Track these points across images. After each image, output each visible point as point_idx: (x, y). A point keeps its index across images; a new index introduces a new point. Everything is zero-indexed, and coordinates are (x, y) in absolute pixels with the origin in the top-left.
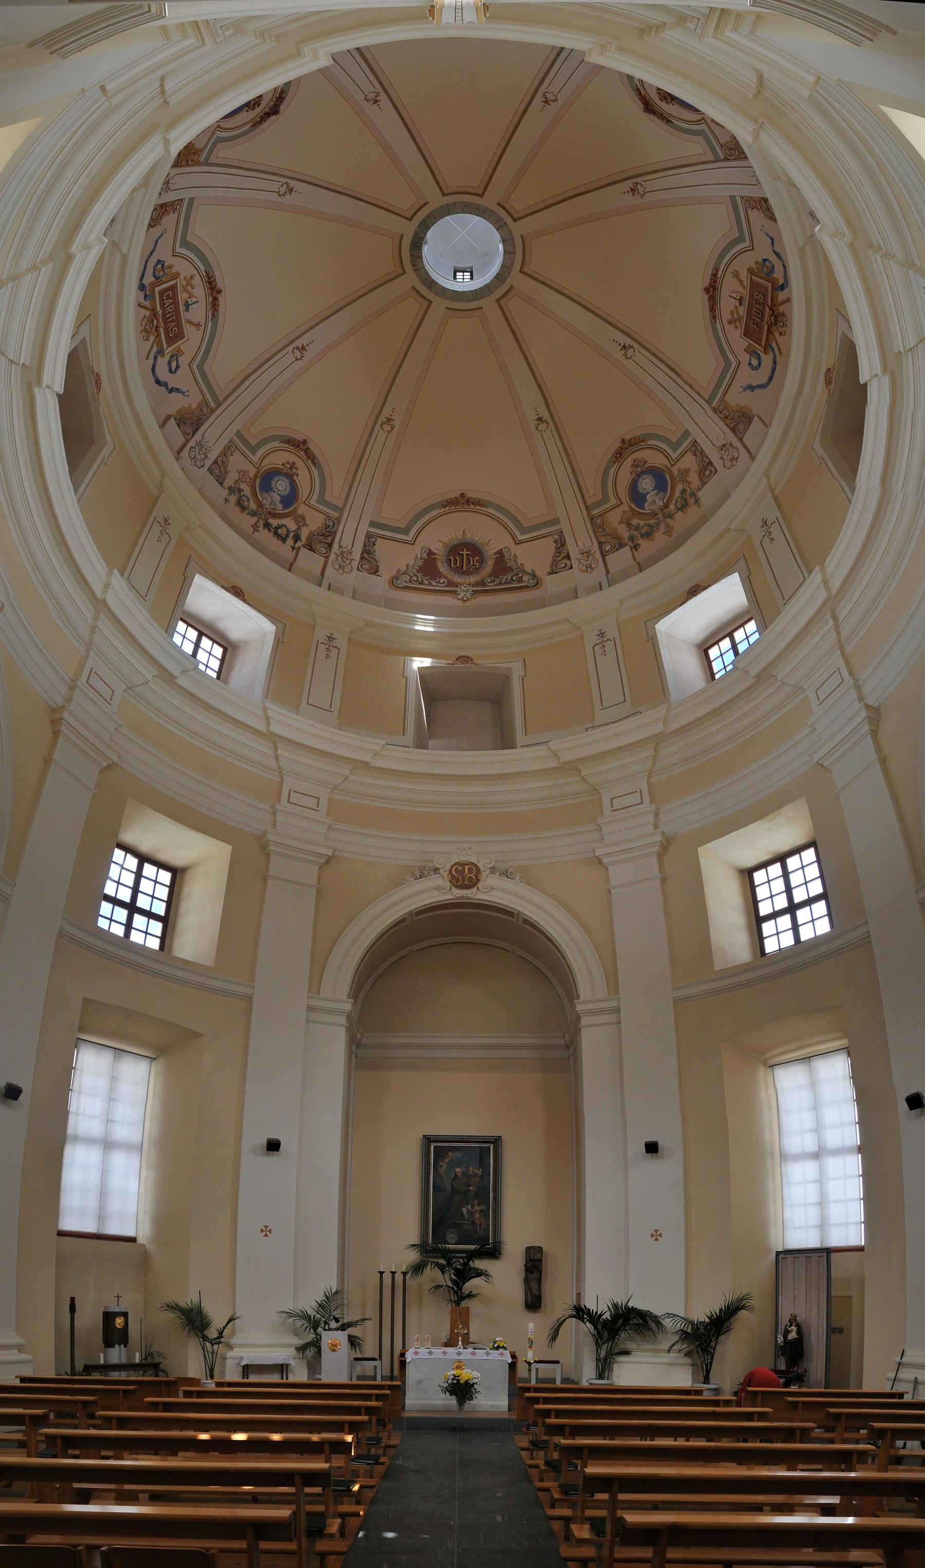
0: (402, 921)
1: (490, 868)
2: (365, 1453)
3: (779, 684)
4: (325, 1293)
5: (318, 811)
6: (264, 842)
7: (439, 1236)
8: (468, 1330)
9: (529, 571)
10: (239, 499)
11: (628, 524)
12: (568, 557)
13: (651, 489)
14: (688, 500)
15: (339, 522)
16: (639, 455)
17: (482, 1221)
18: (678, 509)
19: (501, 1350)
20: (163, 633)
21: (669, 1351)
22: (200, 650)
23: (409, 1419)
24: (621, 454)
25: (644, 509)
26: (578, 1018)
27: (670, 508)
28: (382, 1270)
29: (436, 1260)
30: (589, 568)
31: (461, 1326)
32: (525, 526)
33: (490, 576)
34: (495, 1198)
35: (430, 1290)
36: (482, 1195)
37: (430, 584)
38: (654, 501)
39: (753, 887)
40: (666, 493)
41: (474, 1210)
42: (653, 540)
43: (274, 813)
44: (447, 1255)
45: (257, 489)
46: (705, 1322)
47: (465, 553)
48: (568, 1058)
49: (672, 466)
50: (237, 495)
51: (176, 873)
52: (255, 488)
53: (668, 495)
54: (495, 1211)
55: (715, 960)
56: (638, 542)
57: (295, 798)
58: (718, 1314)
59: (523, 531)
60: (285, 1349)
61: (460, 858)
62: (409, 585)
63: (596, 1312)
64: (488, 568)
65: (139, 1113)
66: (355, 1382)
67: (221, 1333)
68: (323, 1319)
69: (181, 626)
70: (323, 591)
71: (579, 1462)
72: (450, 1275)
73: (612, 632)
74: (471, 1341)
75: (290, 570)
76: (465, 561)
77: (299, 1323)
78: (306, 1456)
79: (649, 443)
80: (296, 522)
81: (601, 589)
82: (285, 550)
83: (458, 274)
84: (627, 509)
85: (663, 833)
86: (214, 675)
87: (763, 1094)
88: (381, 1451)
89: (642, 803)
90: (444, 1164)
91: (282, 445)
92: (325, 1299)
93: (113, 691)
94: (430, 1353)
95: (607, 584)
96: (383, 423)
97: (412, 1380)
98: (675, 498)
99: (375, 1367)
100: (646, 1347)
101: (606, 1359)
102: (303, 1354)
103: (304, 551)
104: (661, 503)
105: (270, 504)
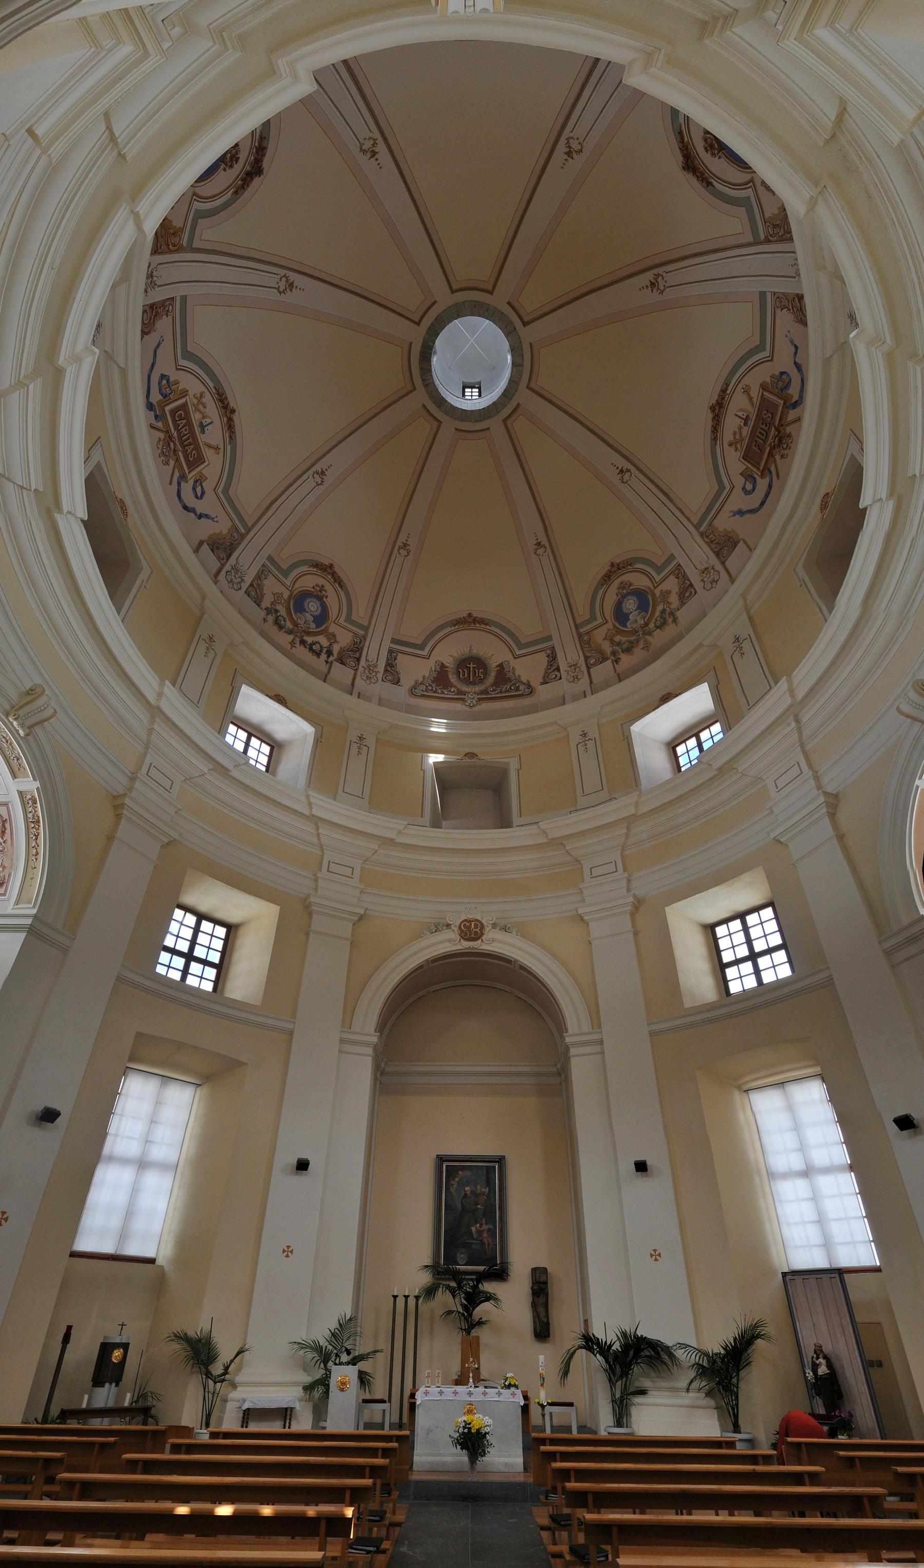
0: (420, 967)
1: (492, 924)
2: (366, 1535)
3: (740, 775)
4: (339, 1320)
5: (352, 878)
6: (307, 903)
7: (450, 1258)
8: (479, 1365)
9: (525, 681)
10: (276, 619)
11: (612, 641)
12: (558, 669)
13: (634, 609)
14: (667, 618)
15: (365, 639)
16: (626, 578)
17: (490, 1240)
18: (657, 627)
19: (513, 1389)
20: (216, 734)
21: (688, 1390)
22: (250, 748)
23: (417, 1482)
24: (609, 577)
25: (627, 627)
26: (567, 1049)
27: (650, 626)
28: (395, 1294)
29: (448, 1283)
30: (576, 679)
31: (471, 1359)
32: (523, 642)
33: (492, 686)
34: (501, 1216)
35: (441, 1316)
36: (489, 1213)
37: (443, 693)
38: (636, 619)
39: (715, 940)
40: (647, 613)
41: (482, 1229)
42: (632, 655)
43: (316, 880)
44: (457, 1276)
45: (292, 609)
46: (720, 1353)
47: (471, 666)
48: (561, 1084)
49: (655, 588)
50: (274, 615)
51: (231, 929)
52: (290, 608)
53: (649, 614)
54: (501, 1230)
55: (684, 1000)
56: (619, 657)
57: (333, 868)
58: (733, 1344)
59: (521, 646)
60: (292, 1388)
61: (468, 916)
62: (425, 693)
63: (606, 1342)
64: (491, 678)
65: (179, 1135)
66: (362, 1431)
67: (226, 1368)
68: (335, 1351)
69: (232, 729)
70: (353, 699)
71: (608, 1548)
72: (461, 1299)
73: (593, 733)
74: (482, 1377)
75: (325, 681)
76: (471, 673)
77: (310, 1355)
78: (298, 1539)
79: (635, 566)
80: (328, 639)
81: (585, 697)
82: (320, 663)
83: (467, 390)
84: (611, 627)
85: (634, 896)
86: (263, 769)
87: (741, 1116)
88: (384, 1532)
89: (617, 871)
90: (454, 1184)
91: (311, 569)
92: (338, 1327)
93: (173, 782)
94: (441, 1393)
95: (590, 692)
96: (400, 548)
97: (421, 1429)
98: (655, 617)
99: (384, 1411)
100: (663, 1384)
101: (622, 1399)
102: (310, 1395)
103: (336, 664)
104: (642, 622)
105: (304, 623)
